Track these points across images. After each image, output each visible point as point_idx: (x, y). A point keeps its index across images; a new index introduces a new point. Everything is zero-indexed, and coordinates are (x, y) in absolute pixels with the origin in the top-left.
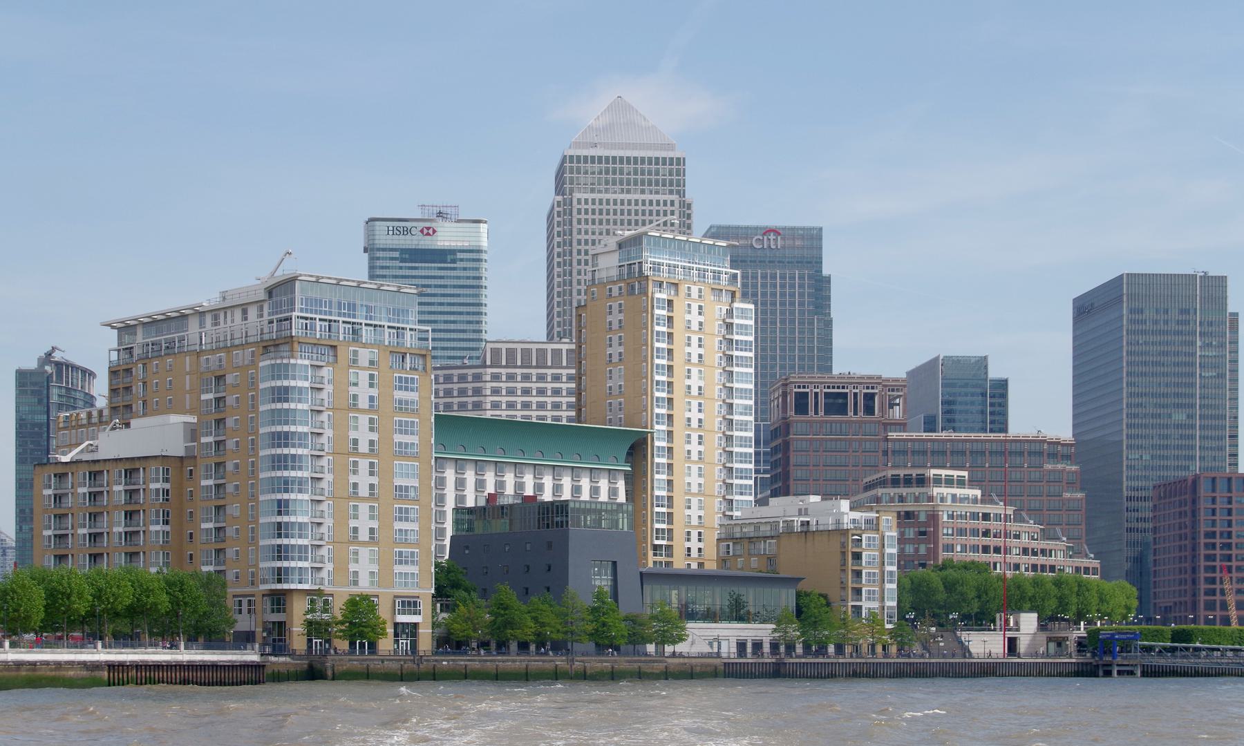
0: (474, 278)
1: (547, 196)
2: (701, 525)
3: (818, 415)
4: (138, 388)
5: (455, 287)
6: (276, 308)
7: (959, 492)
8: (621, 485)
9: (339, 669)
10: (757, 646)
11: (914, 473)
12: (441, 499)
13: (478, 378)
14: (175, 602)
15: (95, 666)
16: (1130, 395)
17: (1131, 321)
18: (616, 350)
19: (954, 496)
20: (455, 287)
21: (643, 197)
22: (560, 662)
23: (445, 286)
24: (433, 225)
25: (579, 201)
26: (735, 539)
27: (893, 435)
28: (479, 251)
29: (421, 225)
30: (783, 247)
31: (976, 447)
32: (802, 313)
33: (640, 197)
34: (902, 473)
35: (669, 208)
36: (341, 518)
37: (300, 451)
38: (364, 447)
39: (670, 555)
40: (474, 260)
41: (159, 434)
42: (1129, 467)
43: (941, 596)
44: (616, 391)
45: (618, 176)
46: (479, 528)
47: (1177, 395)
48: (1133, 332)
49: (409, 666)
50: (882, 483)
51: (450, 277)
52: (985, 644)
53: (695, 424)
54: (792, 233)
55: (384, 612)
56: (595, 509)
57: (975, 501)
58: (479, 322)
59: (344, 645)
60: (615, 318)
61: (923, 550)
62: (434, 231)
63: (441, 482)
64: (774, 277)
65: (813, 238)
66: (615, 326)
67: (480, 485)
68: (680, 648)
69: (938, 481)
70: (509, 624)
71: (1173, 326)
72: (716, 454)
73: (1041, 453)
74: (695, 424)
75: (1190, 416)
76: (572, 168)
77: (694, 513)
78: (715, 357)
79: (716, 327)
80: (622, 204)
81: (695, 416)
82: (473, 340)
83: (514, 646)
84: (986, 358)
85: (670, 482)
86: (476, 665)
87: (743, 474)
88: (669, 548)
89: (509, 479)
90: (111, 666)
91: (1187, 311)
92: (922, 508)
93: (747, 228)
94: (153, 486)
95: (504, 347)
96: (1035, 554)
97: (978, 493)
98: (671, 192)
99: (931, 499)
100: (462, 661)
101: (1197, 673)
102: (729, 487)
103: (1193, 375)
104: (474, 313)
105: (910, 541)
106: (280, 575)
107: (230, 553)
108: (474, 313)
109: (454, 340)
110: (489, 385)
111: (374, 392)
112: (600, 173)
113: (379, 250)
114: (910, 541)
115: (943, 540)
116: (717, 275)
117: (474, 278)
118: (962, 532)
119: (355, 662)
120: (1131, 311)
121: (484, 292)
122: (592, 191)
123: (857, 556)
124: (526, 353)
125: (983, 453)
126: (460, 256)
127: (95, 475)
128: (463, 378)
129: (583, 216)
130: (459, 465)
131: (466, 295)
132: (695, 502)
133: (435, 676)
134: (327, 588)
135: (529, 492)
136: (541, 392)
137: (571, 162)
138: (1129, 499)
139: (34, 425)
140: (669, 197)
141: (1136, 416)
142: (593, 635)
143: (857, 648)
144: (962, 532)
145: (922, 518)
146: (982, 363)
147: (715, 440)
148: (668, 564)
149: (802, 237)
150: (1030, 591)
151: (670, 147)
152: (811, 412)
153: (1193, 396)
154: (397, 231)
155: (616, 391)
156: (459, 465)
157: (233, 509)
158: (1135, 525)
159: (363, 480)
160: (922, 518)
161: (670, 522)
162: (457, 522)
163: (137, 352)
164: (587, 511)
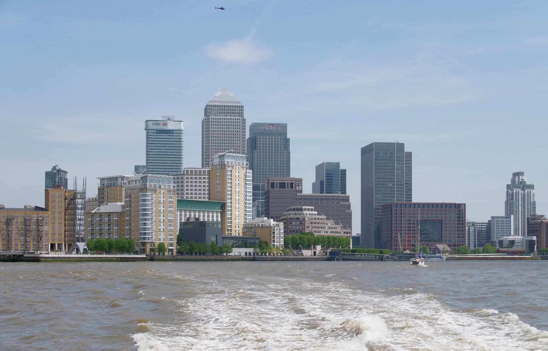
1: (202, 116)
4: (106, 193)
7: (311, 212)
8: (219, 215)
10: (250, 253)
13: (182, 178)
14: (130, 246)
15: (118, 258)
16: (376, 178)
17: (376, 157)
18: (218, 182)
22: (204, 257)
26: (247, 228)
27: (298, 194)
28: (181, 130)
29: (163, 122)
31: (321, 198)
32: (281, 150)
34: (296, 207)
35: (239, 121)
36: (157, 226)
38: (162, 211)
39: (231, 231)
41: (116, 207)
42: (376, 200)
43: (299, 241)
46: (186, 227)
47: (390, 178)
50: (291, 210)
52: (307, 253)
53: (237, 200)
54: (278, 125)
55: (166, 246)
56: (213, 223)
57: (315, 215)
58: (181, 152)
60: (218, 174)
61: (301, 228)
64: (272, 139)
67: (185, 215)
68: (231, 254)
69: (305, 209)
70: (193, 249)
73: (339, 199)
74: (237, 200)
77: (237, 221)
78: (242, 183)
79: (242, 176)
81: (237, 198)
83: (194, 254)
87: (249, 212)
88: (231, 230)
89: (192, 214)
90: (120, 258)
91: (392, 154)
92: (301, 217)
95: (190, 170)
97: (316, 213)
99: (303, 214)
100: (183, 257)
101: (351, 260)
105: (298, 225)
106: (144, 238)
107: (132, 234)
111: (164, 199)
114: (298, 225)
115: (307, 225)
116: (243, 164)
119: (160, 257)
120: (376, 154)
121: (182, 143)
122: (216, 115)
123: (274, 233)
124: (196, 171)
126: (175, 132)
127: (100, 216)
132: (237, 219)
133: (177, 260)
135: (197, 217)
136: (200, 182)
138: (375, 209)
141: (377, 184)
142: (212, 251)
143: (274, 254)
144: (312, 223)
145: (301, 219)
146: (338, 164)
147: (242, 203)
148: (231, 234)
149: (281, 127)
150: (321, 240)
151: (239, 102)
152: (275, 188)
153: (394, 178)
154: (155, 124)
157: (133, 224)
159: (162, 218)
160: (301, 219)
163: (105, 185)
164: (210, 223)
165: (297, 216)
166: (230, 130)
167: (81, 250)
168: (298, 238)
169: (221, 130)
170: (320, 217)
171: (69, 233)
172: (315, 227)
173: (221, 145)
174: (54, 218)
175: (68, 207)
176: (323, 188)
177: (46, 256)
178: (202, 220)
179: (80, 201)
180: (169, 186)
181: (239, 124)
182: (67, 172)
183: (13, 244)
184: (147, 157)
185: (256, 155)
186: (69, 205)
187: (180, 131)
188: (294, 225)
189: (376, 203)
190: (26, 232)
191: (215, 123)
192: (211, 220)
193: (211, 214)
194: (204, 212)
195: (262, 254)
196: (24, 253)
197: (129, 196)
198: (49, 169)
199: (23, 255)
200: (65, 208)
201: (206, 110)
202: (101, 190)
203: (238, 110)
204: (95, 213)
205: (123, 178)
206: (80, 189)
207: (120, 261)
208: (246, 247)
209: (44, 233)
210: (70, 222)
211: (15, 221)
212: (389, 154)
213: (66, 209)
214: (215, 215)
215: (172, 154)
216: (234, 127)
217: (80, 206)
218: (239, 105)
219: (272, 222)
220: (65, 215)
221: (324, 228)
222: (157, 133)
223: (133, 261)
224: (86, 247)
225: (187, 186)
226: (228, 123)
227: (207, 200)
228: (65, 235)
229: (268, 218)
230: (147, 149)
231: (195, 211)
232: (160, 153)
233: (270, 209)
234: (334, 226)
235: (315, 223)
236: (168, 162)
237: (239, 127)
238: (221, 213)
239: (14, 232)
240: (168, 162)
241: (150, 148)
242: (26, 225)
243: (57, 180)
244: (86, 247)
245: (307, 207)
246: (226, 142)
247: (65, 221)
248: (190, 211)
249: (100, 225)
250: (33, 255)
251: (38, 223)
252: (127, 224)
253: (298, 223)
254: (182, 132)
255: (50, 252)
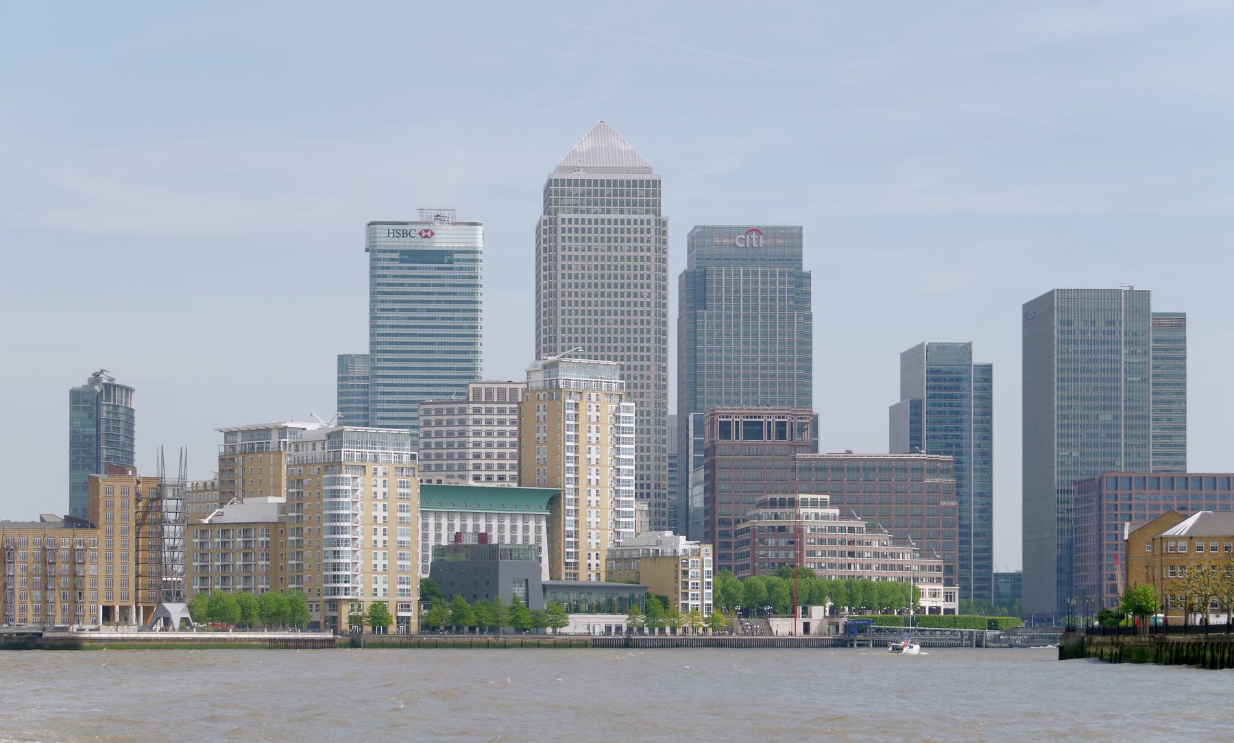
0: (470, 277)
1: (535, 212)
2: (598, 549)
3: (737, 440)
4: (239, 471)
5: (452, 285)
6: (332, 445)
7: (820, 511)
8: (544, 524)
9: (368, 642)
10: (619, 628)
11: (787, 497)
12: (425, 537)
13: (462, 411)
14: (294, 610)
15: (264, 640)
16: (1061, 398)
19: (817, 515)
20: (452, 285)
21: (622, 216)
22: (491, 638)
23: (442, 285)
24: (431, 227)
25: (563, 221)
26: (618, 558)
27: (800, 455)
28: (475, 252)
29: (420, 228)
30: (765, 246)
32: (782, 308)
33: (619, 217)
34: (778, 497)
37: (346, 524)
39: (577, 568)
40: (470, 260)
42: (1061, 463)
43: (765, 594)
44: (542, 462)
45: (599, 198)
48: (1065, 342)
49: (405, 640)
50: (763, 504)
51: (447, 277)
52: (782, 626)
53: (593, 483)
55: (391, 611)
59: (370, 629)
60: (541, 414)
61: (792, 555)
62: (432, 234)
63: (425, 526)
65: (793, 236)
66: (541, 419)
67: (451, 527)
68: (564, 630)
69: (805, 503)
70: (461, 617)
71: (1100, 336)
72: (608, 502)
73: (921, 470)
75: (1116, 417)
76: (556, 191)
77: (593, 540)
78: (608, 438)
79: (608, 419)
80: (596, 223)
81: (594, 477)
82: (468, 336)
84: (970, 344)
85: (576, 521)
86: (442, 640)
88: (576, 564)
89: (470, 523)
90: (271, 640)
91: (1112, 323)
92: (790, 524)
93: (730, 227)
94: (260, 539)
96: (885, 556)
97: (837, 512)
98: (648, 212)
99: (798, 517)
100: (434, 638)
102: (617, 523)
103: (1118, 380)
104: (470, 311)
105: (782, 548)
106: (336, 591)
108: (470, 311)
109: (450, 335)
110: (471, 417)
112: (583, 195)
113: (380, 251)
114: (782, 548)
115: (807, 548)
116: (609, 385)
117: (470, 277)
118: (822, 541)
119: (376, 638)
120: (1061, 323)
121: (479, 290)
122: (576, 211)
123: (686, 573)
125: (873, 469)
126: (456, 256)
127: (224, 532)
128: (450, 411)
129: (567, 235)
130: (438, 515)
131: (463, 294)
132: (593, 534)
133: (419, 645)
134: (360, 598)
135: (482, 530)
137: (556, 185)
139: (85, 437)
140: (645, 217)
141: (1065, 417)
142: (512, 623)
144: (822, 541)
145: (792, 531)
146: (967, 349)
147: (608, 493)
149: (784, 236)
151: (648, 170)
152: (733, 437)
153: (1119, 399)
154: (397, 234)
155: (542, 462)
156: (438, 515)
157: (308, 554)
158: (1065, 515)
160: (792, 531)
161: (577, 547)
162: (434, 554)
163: (238, 449)
165: (782, 523)
166: (619, 254)
167: (176, 622)
168: (762, 586)
169: (593, 253)
170: (847, 524)
171: (147, 581)
172: (833, 554)
173: (593, 299)
174: (111, 545)
175: (144, 519)
176: (920, 422)
177: (95, 635)
178: (495, 541)
179: (172, 503)
180: (400, 457)
181: (645, 236)
182: (132, 390)
183: (17, 606)
184: (372, 335)
185: (705, 323)
186: (146, 513)
187: (471, 255)
188: (772, 548)
189: (1061, 473)
190: (45, 581)
191: (573, 235)
192: (520, 541)
193: (520, 524)
194: (501, 517)
195: (652, 631)
196: (44, 629)
197: (296, 481)
198: (81, 381)
199: (40, 635)
200: (137, 520)
201: (547, 192)
202: (226, 462)
203: (642, 194)
204: (211, 524)
205: (283, 431)
206: (171, 476)
207: (270, 648)
208: (611, 612)
209: (87, 581)
210: (147, 555)
211: (19, 553)
212: (1101, 325)
213: (139, 524)
214: (532, 524)
215: (449, 323)
216: (632, 244)
217: (171, 516)
218: (647, 177)
219: (683, 544)
220: (137, 538)
221: (861, 555)
222: (402, 261)
223: (301, 647)
224: (187, 615)
225: (477, 434)
226: (613, 235)
227: (514, 485)
228: (137, 585)
229: (675, 534)
230: (372, 310)
231: (476, 516)
232: (413, 323)
233: (718, 499)
234: (892, 549)
235: (833, 541)
236: (437, 348)
237: (645, 245)
238: (548, 519)
239: (17, 580)
240: (437, 348)
241: (380, 306)
242: (45, 563)
243: (104, 415)
244: (187, 615)
245: (809, 497)
246: (606, 290)
247: (137, 551)
248: (463, 516)
249: (224, 555)
250: (65, 635)
251: (75, 558)
252: (292, 554)
253: (782, 543)
254: (479, 257)
255: (103, 628)
